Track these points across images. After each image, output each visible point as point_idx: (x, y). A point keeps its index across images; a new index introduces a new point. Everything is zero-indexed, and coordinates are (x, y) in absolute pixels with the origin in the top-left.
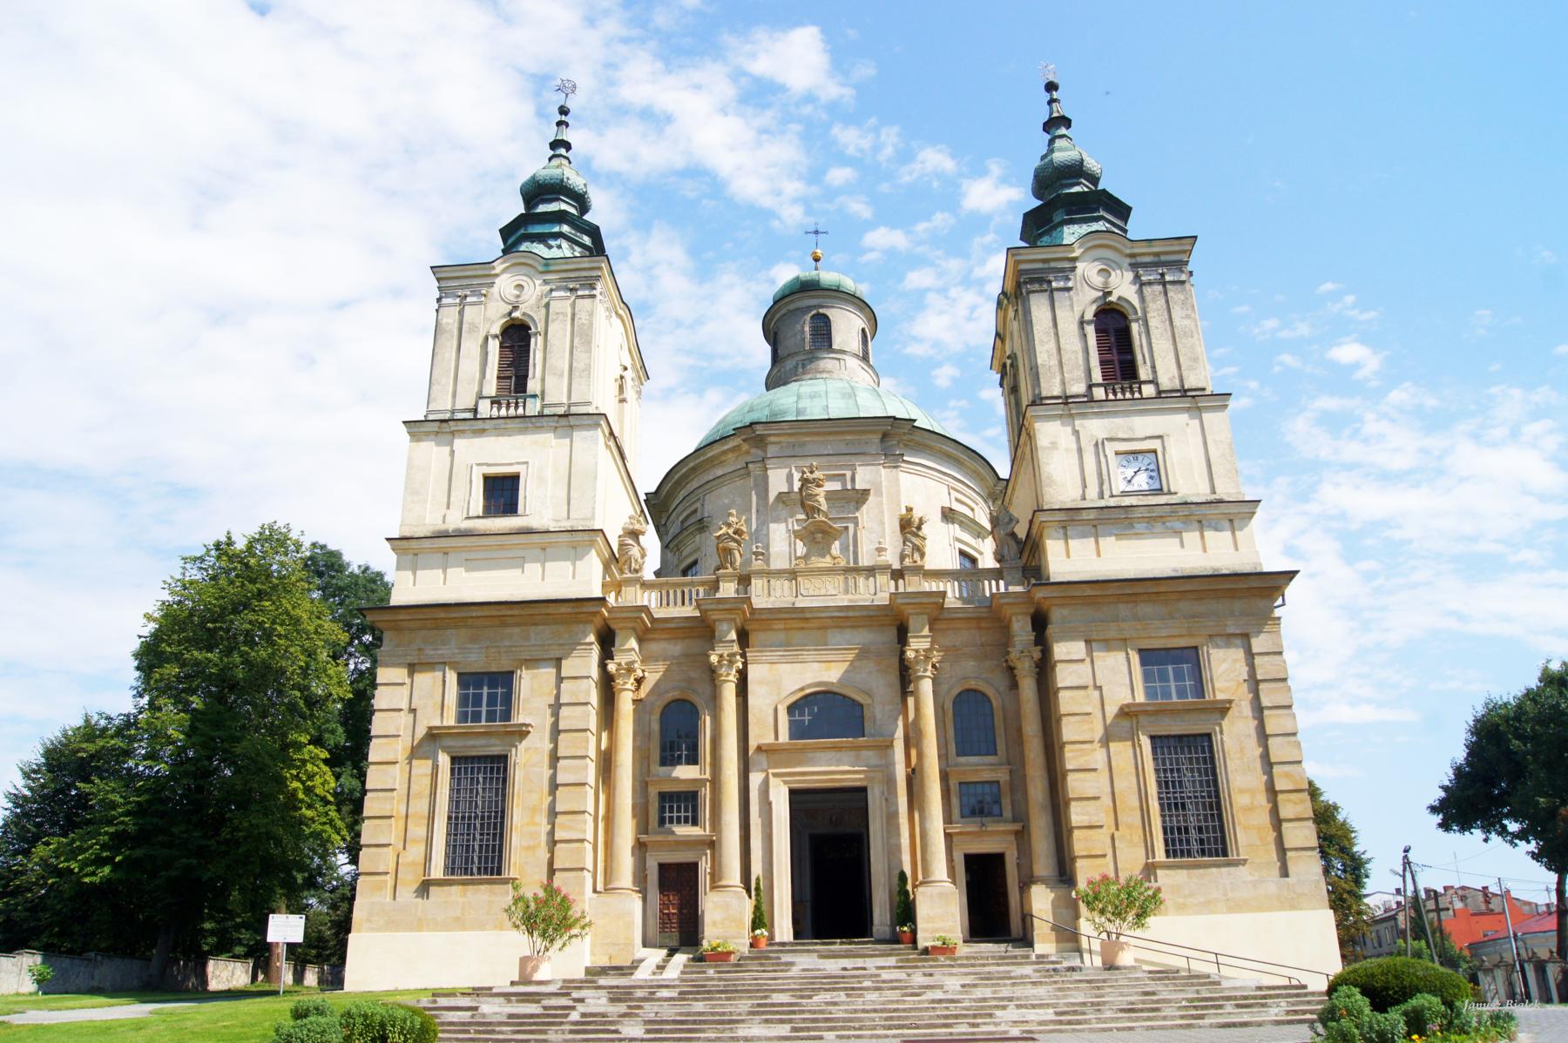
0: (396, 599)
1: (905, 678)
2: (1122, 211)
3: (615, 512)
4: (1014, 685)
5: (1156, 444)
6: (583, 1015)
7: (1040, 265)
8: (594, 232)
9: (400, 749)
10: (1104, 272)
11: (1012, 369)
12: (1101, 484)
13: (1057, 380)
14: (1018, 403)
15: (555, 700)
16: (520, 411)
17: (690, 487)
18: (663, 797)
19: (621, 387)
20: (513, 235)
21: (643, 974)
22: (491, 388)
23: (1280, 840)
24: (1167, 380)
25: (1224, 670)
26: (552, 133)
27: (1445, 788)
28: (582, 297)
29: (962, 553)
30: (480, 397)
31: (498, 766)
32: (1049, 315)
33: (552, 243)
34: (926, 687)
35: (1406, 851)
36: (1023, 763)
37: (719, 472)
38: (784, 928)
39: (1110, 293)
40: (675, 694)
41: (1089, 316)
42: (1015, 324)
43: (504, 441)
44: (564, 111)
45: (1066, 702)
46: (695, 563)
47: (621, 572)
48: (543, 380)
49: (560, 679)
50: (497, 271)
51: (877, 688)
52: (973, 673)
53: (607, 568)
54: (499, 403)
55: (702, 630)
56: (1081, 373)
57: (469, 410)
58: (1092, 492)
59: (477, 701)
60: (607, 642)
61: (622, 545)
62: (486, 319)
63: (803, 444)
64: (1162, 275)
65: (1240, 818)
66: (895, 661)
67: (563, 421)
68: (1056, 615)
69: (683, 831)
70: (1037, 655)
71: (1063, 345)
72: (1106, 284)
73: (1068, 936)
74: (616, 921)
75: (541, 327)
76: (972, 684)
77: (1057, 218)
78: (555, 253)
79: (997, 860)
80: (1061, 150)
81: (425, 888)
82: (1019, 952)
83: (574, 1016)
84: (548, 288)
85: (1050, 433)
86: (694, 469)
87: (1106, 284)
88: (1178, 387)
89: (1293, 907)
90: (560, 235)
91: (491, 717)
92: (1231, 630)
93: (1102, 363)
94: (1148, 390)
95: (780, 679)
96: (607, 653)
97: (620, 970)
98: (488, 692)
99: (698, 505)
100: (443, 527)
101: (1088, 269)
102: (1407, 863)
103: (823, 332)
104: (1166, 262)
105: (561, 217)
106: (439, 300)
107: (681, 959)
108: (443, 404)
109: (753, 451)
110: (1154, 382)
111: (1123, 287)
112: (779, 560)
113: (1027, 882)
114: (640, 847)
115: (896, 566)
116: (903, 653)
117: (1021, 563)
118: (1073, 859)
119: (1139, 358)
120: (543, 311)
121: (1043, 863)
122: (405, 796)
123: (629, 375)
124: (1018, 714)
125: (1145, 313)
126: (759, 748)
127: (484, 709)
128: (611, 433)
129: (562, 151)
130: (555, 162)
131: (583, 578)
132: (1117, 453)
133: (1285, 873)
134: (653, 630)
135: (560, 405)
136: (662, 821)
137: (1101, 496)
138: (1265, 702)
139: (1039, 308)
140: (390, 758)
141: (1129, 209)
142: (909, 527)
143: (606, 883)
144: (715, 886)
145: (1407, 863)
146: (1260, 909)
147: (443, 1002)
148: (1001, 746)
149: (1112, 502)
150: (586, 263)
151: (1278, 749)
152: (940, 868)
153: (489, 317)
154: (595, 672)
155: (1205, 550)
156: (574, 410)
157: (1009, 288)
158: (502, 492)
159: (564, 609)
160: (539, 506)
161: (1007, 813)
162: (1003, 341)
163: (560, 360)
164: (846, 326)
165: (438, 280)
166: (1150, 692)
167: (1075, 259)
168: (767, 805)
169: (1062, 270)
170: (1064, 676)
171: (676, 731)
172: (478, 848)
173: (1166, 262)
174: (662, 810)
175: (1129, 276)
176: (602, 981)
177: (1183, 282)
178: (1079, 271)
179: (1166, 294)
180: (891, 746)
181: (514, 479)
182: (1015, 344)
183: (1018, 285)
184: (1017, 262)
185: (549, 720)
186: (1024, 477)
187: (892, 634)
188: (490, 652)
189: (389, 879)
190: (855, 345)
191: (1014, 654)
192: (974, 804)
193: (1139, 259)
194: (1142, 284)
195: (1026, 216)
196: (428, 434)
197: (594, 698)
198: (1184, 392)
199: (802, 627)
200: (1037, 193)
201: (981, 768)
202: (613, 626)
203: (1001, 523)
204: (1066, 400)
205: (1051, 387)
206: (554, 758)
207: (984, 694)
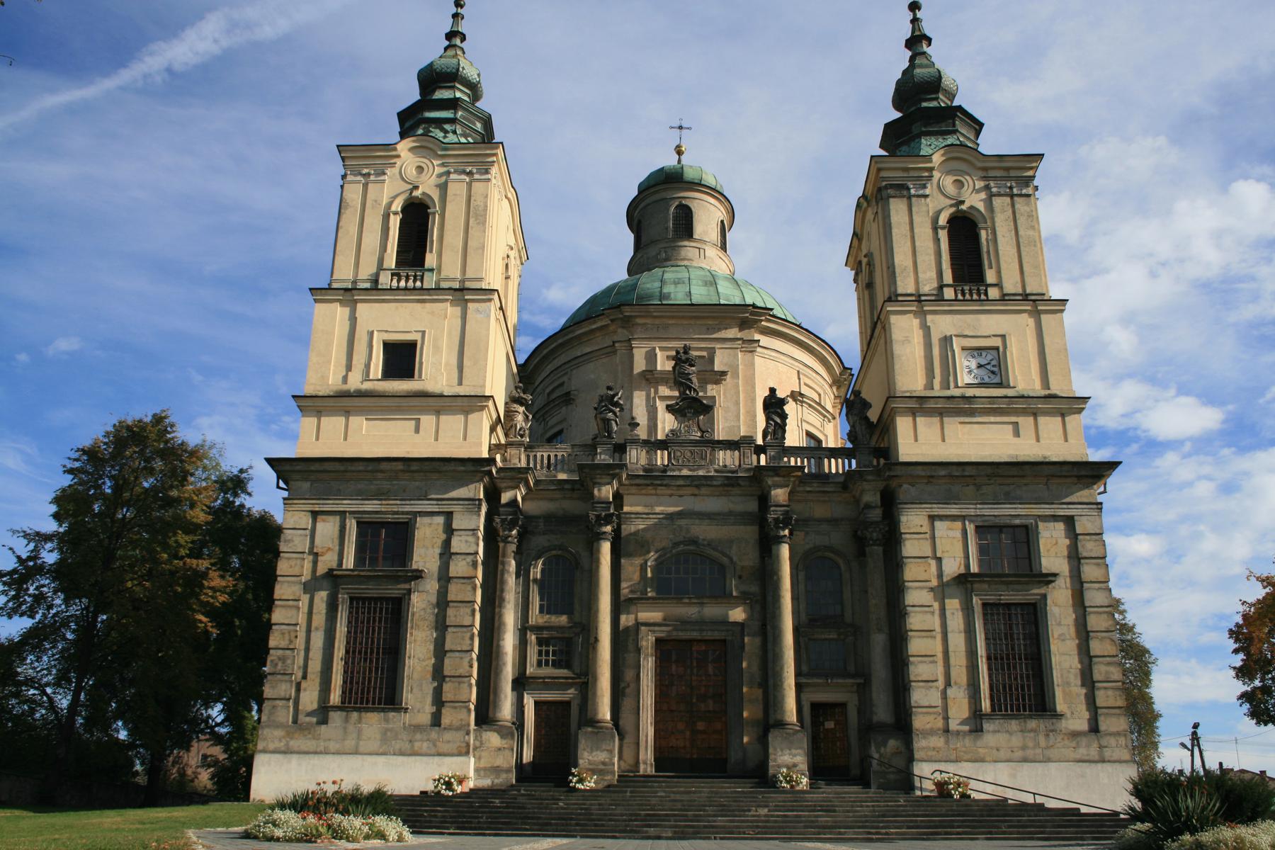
7: (900, 174)
10: (959, 184)
11: (869, 267)
13: (911, 280)
20: (410, 120)
22: (391, 261)
25: (1052, 550)
29: (809, 434)
30: (380, 268)
32: (907, 219)
33: (447, 127)
34: (785, 550)
35: (1196, 726)
39: (962, 202)
41: (943, 220)
42: (875, 226)
46: (560, 432)
63: (666, 327)
64: (1011, 188)
68: (905, 491)
78: (451, 138)
80: (921, 66)
85: (905, 330)
86: (562, 345)
88: (1020, 291)
99: (565, 379)
100: (345, 387)
102: (1195, 738)
103: (685, 224)
104: (1016, 174)
105: (453, 104)
106: (344, 177)
108: (344, 274)
109: (620, 330)
110: (999, 285)
111: (974, 200)
115: (760, 442)
123: (513, 254)
128: (501, 308)
129: (457, 41)
131: (475, 438)
132: (963, 349)
135: (454, 280)
139: (897, 209)
141: (981, 125)
142: (774, 405)
145: (1195, 738)
149: (957, 392)
153: (389, 192)
155: (1038, 440)
156: (468, 285)
158: (401, 358)
160: (435, 372)
163: (453, 238)
164: (707, 216)
165: (343, 159)
167: (931, 169)
173: (1016, 174)
177: (1028, 196)
178: (935, 180)
179: (1013, 205)
182: (873, 243)
184: (879, 170)
186: (877, 365)
188: (381, 504)
190: (714, 235)
193: (992, 173)
195: (887, 126)
198: (1025, 297)
200: (897, 104)
203: (854, 406)
204: (918, 298)
205: (906, 285)
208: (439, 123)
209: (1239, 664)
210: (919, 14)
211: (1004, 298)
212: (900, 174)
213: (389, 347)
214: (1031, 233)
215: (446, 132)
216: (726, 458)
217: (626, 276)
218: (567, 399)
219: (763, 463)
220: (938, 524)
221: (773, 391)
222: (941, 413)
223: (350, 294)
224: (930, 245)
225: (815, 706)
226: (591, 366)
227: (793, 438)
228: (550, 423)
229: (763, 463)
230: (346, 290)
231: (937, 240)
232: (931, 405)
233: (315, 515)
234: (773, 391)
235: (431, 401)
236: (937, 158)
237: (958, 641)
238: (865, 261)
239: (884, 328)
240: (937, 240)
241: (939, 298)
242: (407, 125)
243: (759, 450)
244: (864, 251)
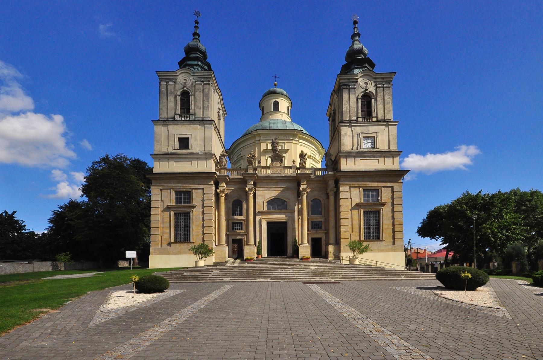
0: (155, 171)
1: (299, 194)
2: (372, 65)
3: (218, 150)
4: (328, 198)
7: (347, 81)
8: (209, 65)
9: (159, 211)
12: (358, 145)
15: (203, 198)
16: (188, 119)
18: (233, 223)
19: (219, 115)
20: (182, 64)
21: (228, 265)
23: (394, 236)
24: (380, 117)
25: (386, 195)
26: (193, 30)
28: (206, 84)
30: (175, 114)
31: (188, 216)
33: (195, 67)
34: (305, 197)
36: (329, 217)
38: (265, 253)
40: (236, 198)
41: (360, 97)
43: (184, 127)
44: (197, 22)
45: (342, 202)
47: (220, 166)
48: (195, 110)
49: (204, 194)
50: (178, 74)
51: (290, 197)
52: (317, 194)
53: (216, 166)
55: (243, 182)
56: (355, 114)
58: (355, 148)
59: (181, 199)
60: (217, 185)
61: (220, 159)
62: (175, 90)
64: (384, 85)
65: (384, 231)
66: (296, 191)
67: (202, 122)
69: (238, 231)
70: (335, 190)
71: (351, 104)
72: (366, 87)
73: (337, 257)
74: (221, 252)
75: (193, 93)
76: (316, 197)
77: (353, 67)
81: (169, 244)
82: (324, 260)
84: (194, 80)
87: (366, 87)
89: (395, 251)
90: (197, 65)
91: (185, 203)
93: (362, 111)
94: (374, 119)
95: (265, 195)
96: (217, 187)
97: (222, 264)
98: (184, 197)
101: (361, 81)
106: (160, 83)
107: (238, 261)
108: (164, 116)
110: (377, 117)
111: (371, 88)
112: (263, 164)
113: (327, 244)
114: (227, 235)
115: (298, 166)
116: (299, 189)
117: (332, 166)
118: (340, 239)
119: (373, 110)
120: (193, 88)
122: (161, 222)
123: (221, 111)
124: (328, 206)
125: (377, 96)
126: (259, 212)
127: (183, 201)
128: (216, 127)
130: (195, 40)
131: (210, 166)
132: (363, 137)
133: (394, 243)
134: (229, 182)
135: (200, 117)
136: (233, 229)
137: (357, 149)
138: (395, 203)
139: (345, 96)
140: (157, 213)
143: (219, 243)
144: (247, 244)
145: (409, 243)
146: (387, 252)
147: (173, 272)
148: (323, 213)
149: (360, 150)
150: (206, 73)
151: (397, 215)
152: (306, 241)
154: (214, 192)
156: (204, 119)
157: (336, 88)
158: (184, 142)
160: (195, 146)
161: (323, 228)
162: (331, 106)
165: (159, 76)
166: (364, 200)
168: (261, 226)
169: (353, 82)
170: (342, 196)
171: (236, 206)
172: (183, 234)
174: (233, 226)
175: (373, 84)
176: (218, 267)
180: (294, 212)
181: (188, 139)
183: (339, 86)
184: (340, 79)
185: (201, 203)
187: (296, 184)
189: (159, 242)
191: (329, 190)
192: (314, 226)
194: (377, 87)
196: (160, 125)
197: (214, 198)
198: (384, 120)
199: (269, 181)
201: (317, 218)
202: (219, 180)
204: (350, 121)
205: (346, 118)
206: (203, 213)
207: (319, 200)
208: (192, 66)
209: (420, 226)
211: (378, 121)
212: (347, 81)
215: (195, 69)
216: (288, 172)
220: (351, 189)
222: (355, 157)
223: (166, 122)
224: (355, 106)
227: (308, 166)
230: (164, 121)
231: (357, 103)
233: (161, 190)
234: (302, 151)
235: (195, 156)
236: (360, 75)
237: (356, 222)
239: (338, 132)
240: (357, 103)
241: (357, 121)
243: (298, 169)
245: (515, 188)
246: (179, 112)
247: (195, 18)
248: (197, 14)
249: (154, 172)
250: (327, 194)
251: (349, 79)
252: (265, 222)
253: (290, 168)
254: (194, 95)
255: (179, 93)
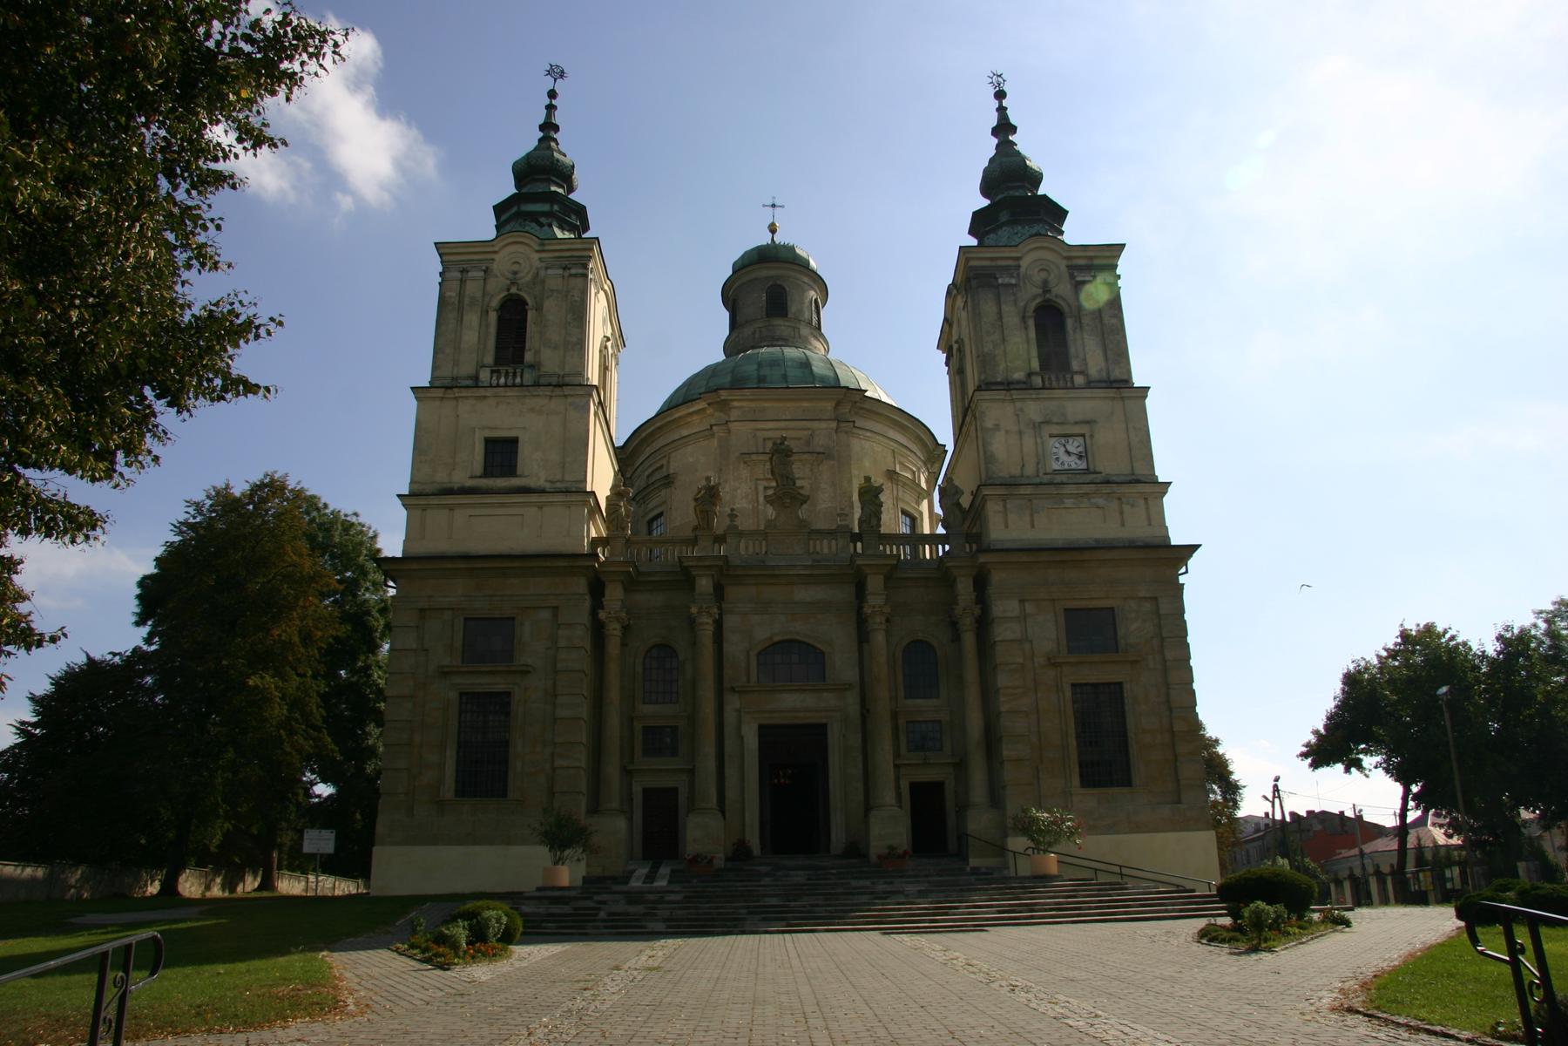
4: (957, 638)
5: (1084, 429)
6: (610, 914)
7: (987, 263)
14: (963, 385)
16: (518, 380)
17: (656, 445)
27: (1316, 732)
28: (575, 275)
33: (543, 220)
35: (1277, 779)
37: (685, 433)
42: (964, 314)
54: (498, 372)
57: (470, 378)
67: (558, 391)
68: (997, 577)
70: (977, 611)
79: (938, 787)
83: (602, 915)
92: (1142, 594)
99: (664, 462)
102: (1276, 789)
109: (718, 414)
121: (978, 794)
142: (870, 496)
145: (1276, 789)
146: (1157, 830)
152: (888, 796)
156: (567, 380)
159: (561, 563)
162: (951, 325)
170: (1004, 632)
181: (514, 442)
183: (968, 280)
184: (968, 260)
191: (958, 610)
195: (975, 214)
200: (987, 188)
210: (1005, 103)
213: (489, 442)
214: (1114, 321)
217: (722, 357)
218: (668, 481)
219: (859, 550)
221: (868, 479)
225: (914, 787)
226: (689, 449)
228: (651, 505)
229: (859, 550)
230: (447, 388)
232: (1022, 491)
234: (868, 479)
235: (534, 498)
238: (955, 347)
242: (504, 218)
243: (856, 538)
244: (955, 338)
245: (221, 485)
246: (489, 359)
247: (549, 83)
248: (557, 73)
249: (883, 530)
250: (954, 625)
251: (992, 259)
252: (755, 727)
253: (832, 534)
254: (539, 309)
255: (495, 303)
